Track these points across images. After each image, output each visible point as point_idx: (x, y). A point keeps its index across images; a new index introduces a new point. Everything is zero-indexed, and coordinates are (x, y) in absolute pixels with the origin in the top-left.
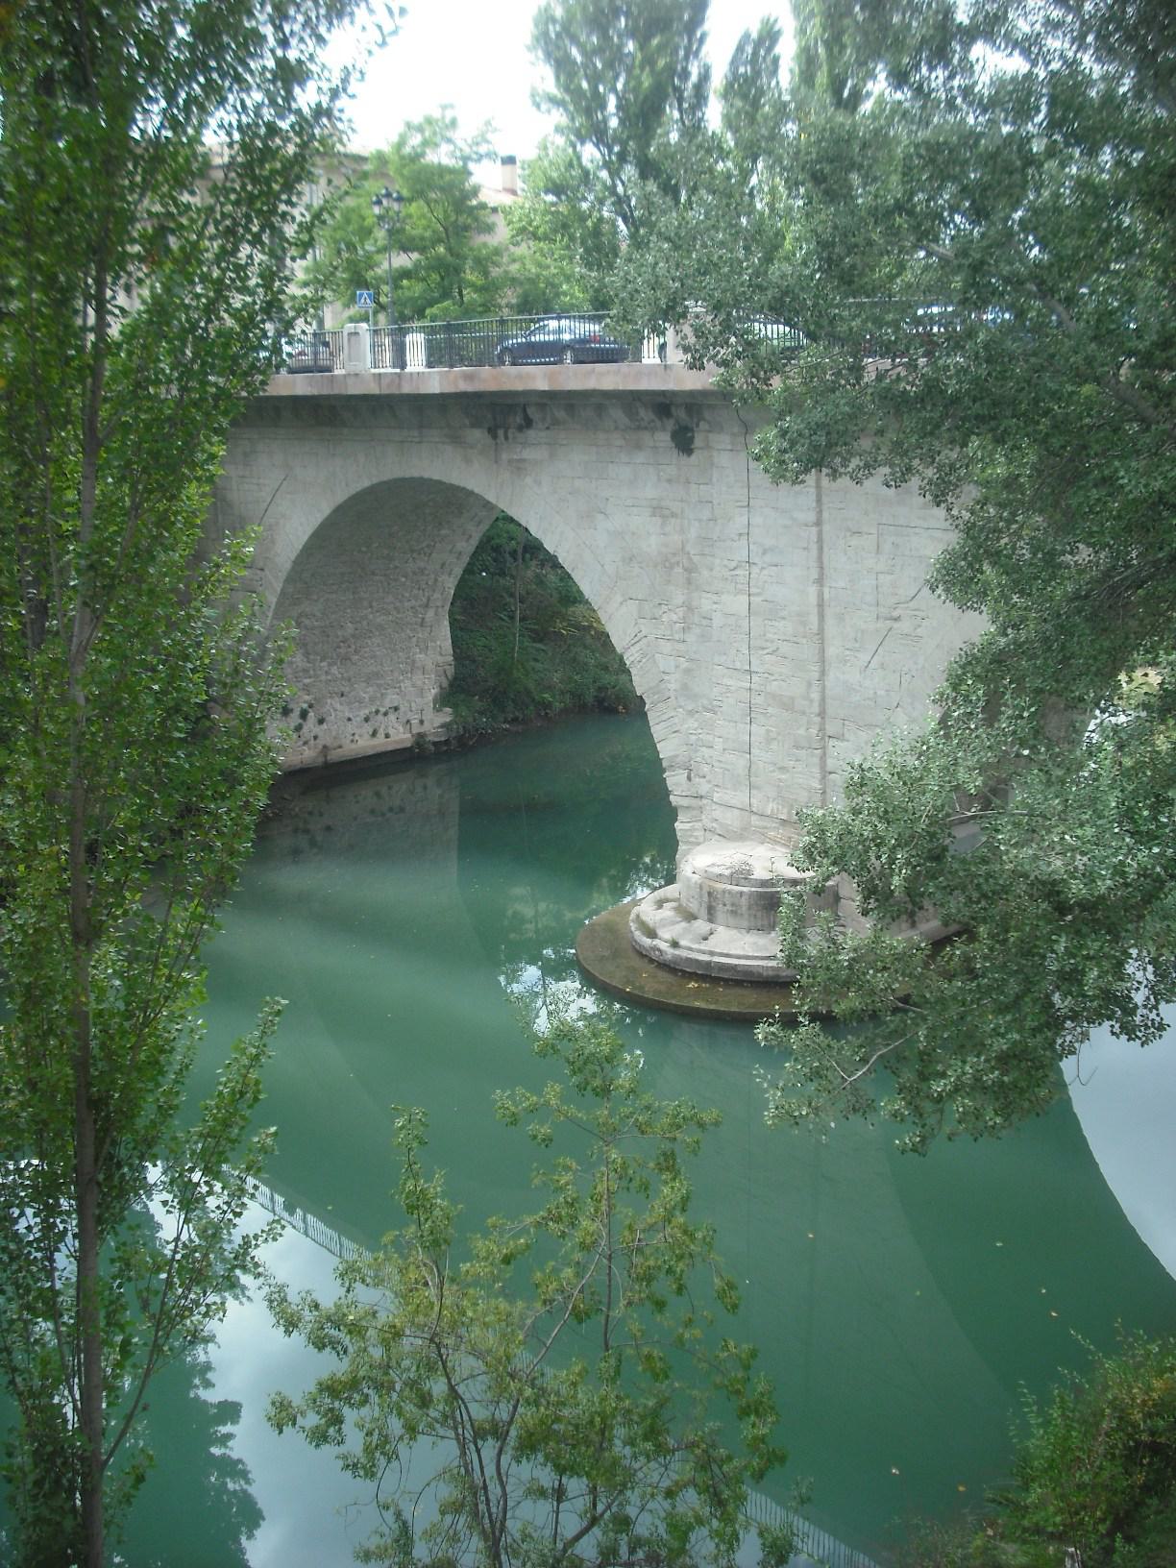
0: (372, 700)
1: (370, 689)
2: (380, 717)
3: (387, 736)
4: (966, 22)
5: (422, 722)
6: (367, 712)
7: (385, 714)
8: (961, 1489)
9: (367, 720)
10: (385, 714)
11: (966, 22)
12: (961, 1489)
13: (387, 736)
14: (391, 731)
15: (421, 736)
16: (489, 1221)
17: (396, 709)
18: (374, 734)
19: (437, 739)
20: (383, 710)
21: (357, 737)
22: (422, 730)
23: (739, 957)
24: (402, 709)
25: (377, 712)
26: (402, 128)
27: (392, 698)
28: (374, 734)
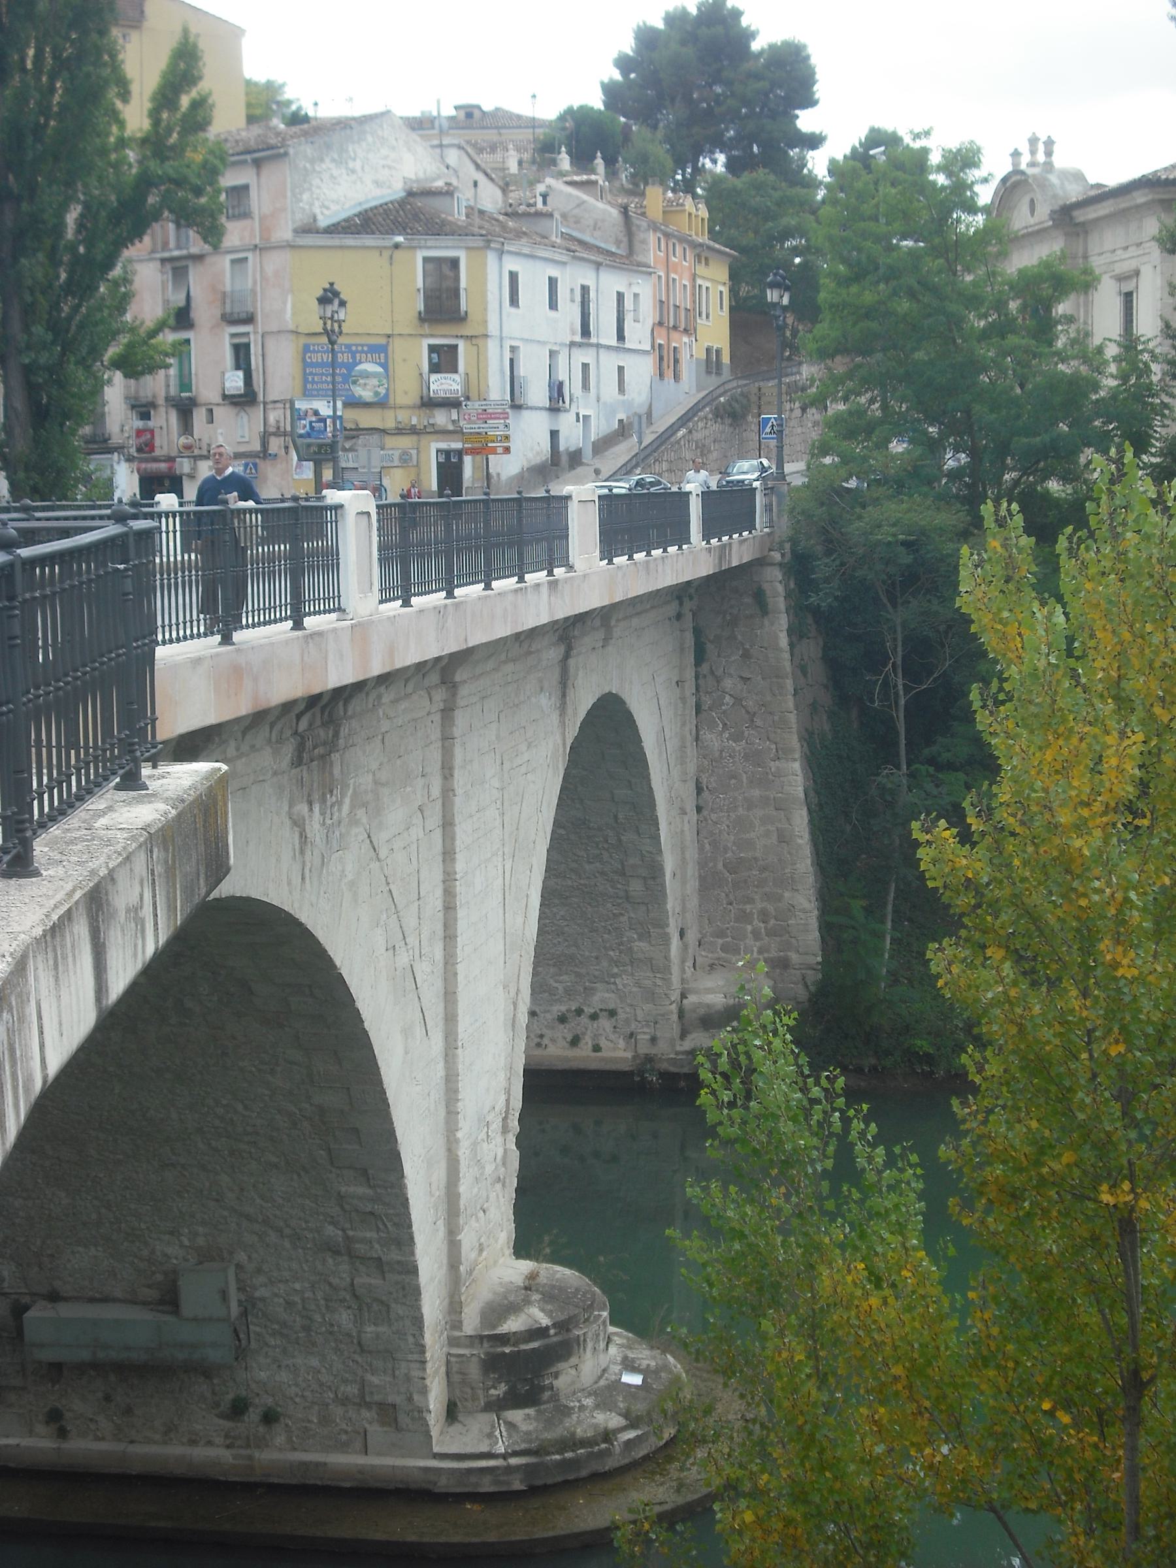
0: (569, 993)
1: (565, 977)
2: (584, 1019)
3: (597, 1048)
4: (503, 1385)
5: (653, 1040)
6: (563, 1008)
7: (594, 1017)
8: (755, 149)
9: (562, 1019)
10: (594, 1017)
11: (503, 1385)
12: (755, 149)
13: (597, 1048)
14: (603, 1043)
15: (649, 1059)
16: (873, 1125)
17: (612, 1013)
18: (575, 1041)
19: (673, 1069)
20: (588, 1010)
21: (546, 1041)
22: (653, 1051)
23: (598, 376)
24: (622, 1015)
25: (579, 1012)
26: (1010, 160)
27: (602, 997)
28: (575, 1041)
